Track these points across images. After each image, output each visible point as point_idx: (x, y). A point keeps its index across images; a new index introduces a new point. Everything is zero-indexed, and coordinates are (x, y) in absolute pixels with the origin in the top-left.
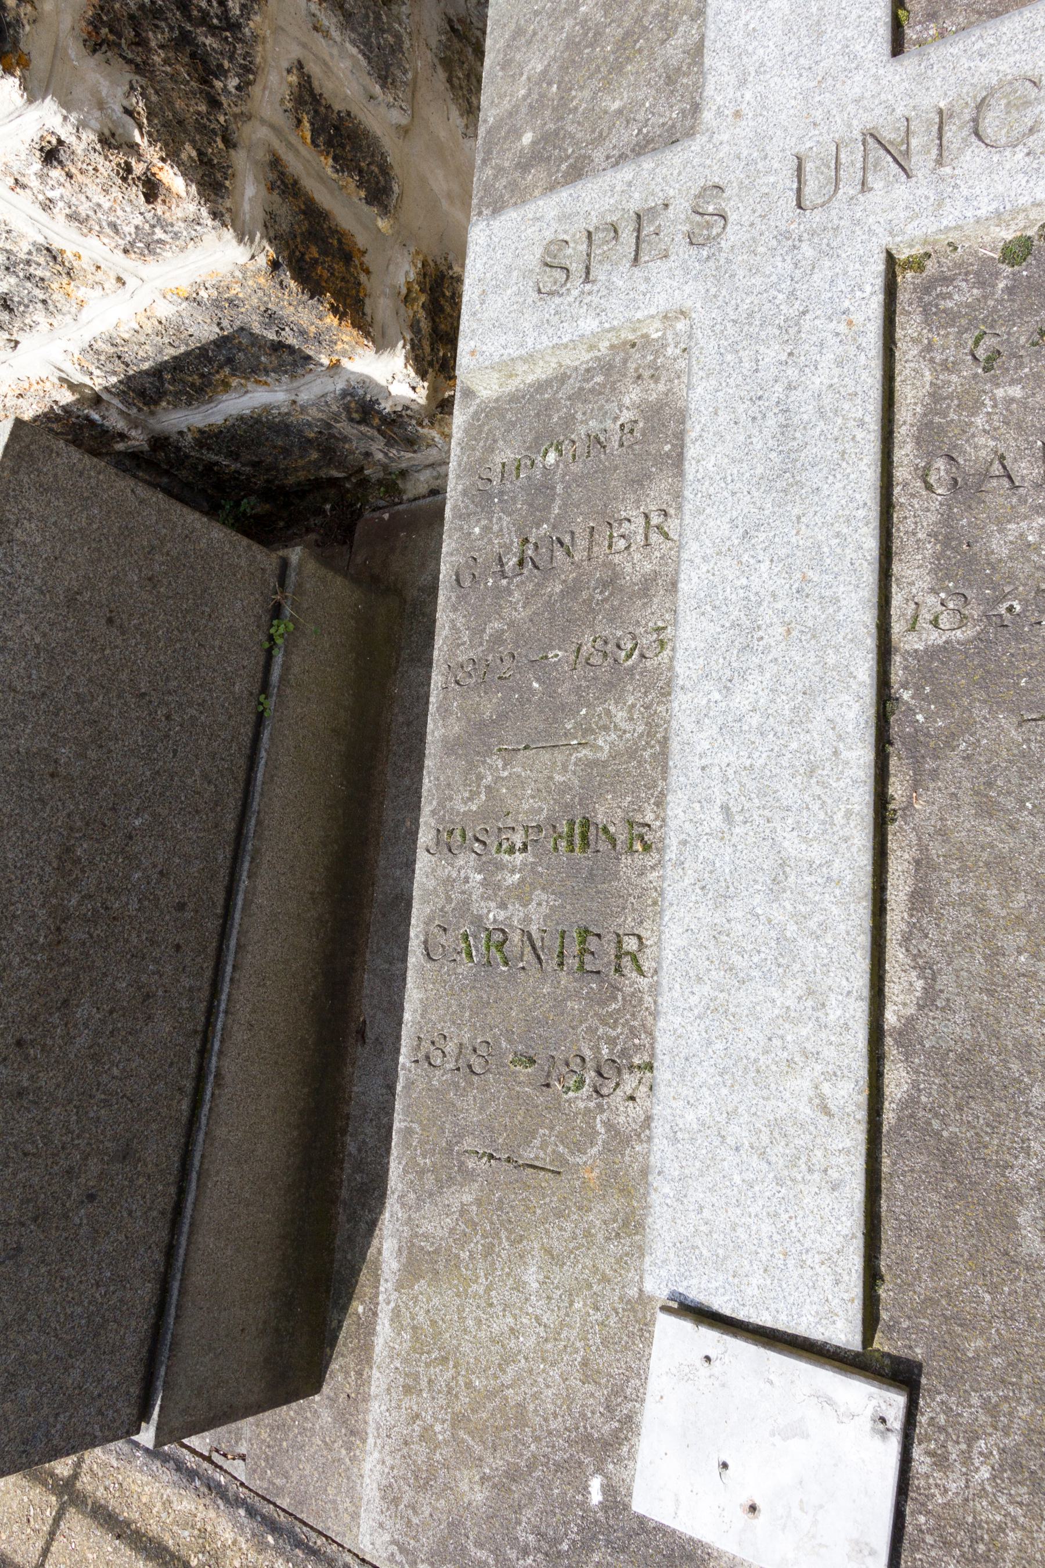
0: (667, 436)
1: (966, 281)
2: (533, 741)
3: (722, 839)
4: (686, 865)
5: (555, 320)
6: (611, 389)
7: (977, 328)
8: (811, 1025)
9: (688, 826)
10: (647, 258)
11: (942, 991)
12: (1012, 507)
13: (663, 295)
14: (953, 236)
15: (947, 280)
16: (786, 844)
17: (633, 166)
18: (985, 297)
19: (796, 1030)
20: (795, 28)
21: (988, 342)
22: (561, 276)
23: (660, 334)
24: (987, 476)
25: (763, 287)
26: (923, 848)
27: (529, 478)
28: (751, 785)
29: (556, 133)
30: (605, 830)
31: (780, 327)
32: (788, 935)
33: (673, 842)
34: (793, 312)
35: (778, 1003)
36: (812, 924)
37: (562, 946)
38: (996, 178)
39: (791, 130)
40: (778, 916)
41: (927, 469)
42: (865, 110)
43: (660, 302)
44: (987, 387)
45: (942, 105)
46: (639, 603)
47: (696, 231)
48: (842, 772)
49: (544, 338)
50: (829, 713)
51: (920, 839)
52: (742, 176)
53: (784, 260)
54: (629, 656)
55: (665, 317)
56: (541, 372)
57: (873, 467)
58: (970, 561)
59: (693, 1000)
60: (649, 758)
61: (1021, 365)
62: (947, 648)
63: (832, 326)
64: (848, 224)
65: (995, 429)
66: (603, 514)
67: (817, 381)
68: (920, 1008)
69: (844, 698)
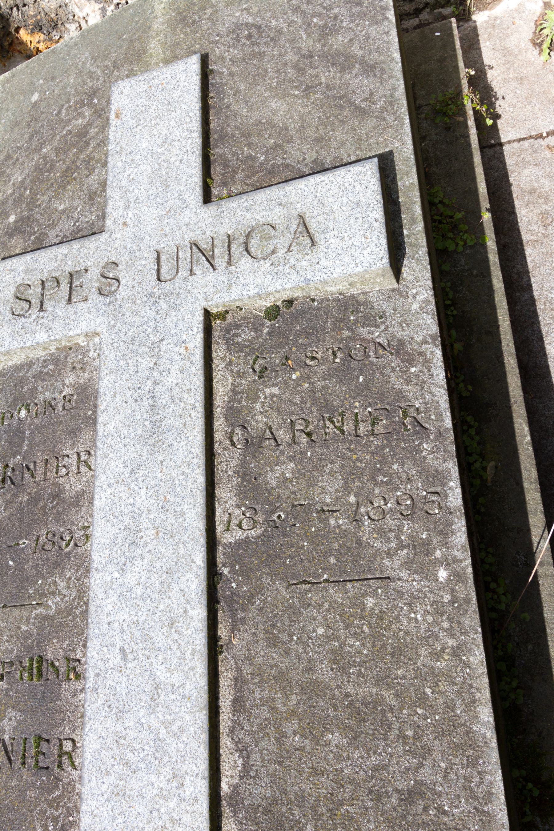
0: (90, 406)
1: (248, 327)
2: (9, 602)
3: (121, 671)
4: (99, 691)
5: (22, 332)
6: (58, 373)
7: (254, 354)
8: (175, 800)
9: (100, 663)
10: (75, 300)
11: (253, 765)
12: (277, 457)
13: (85, 322)
14: (238, 304)
15: (238, 326)
16: (158, 673)
17: (68, 246)
18: (257, 337)
19: (166, 804)
20: (154, 181)
21: (260, 362)
22: (25, 305)
23: (85, 343)
24: (264, 438)
25: (140, 324)
26: (239, 670)
27: (9, 425)
28: (137, 634)
29: (29, 218)
30: (52, 664)
31: (149, 348)
32: (161, 736)
33: (90, 674)
34: (156, 339)
35: (156, 785)
36: (175, 728)
37: (25, 751)
38: (257, 275)
39: (153, 237)
40: (155, 724)
41: (232, 433)
42: (191, 230)
43: (83, 327)
44: (261, 387)
45: (229, 232)
46: (74, 510)
47: (103, 287)
48: (189, 624)
49: (15, 342)
50: (181, 585)
51: (236, 664)
52: (128, 259)
53: (151, 309)
54: (67, 545)
55: (86, 335)
56: (15, 361)
57: (201, 433)
58: (257, 488)
59: (104, 788)
60: (74, 619)
61: (277, 376)
62: (247, 540)
63: (177, 349)
64: (184, 292)
65: (266, 411)
66: (53, 451)
67: (170, 380)
68: (241, 778)
69: (189, 576)
